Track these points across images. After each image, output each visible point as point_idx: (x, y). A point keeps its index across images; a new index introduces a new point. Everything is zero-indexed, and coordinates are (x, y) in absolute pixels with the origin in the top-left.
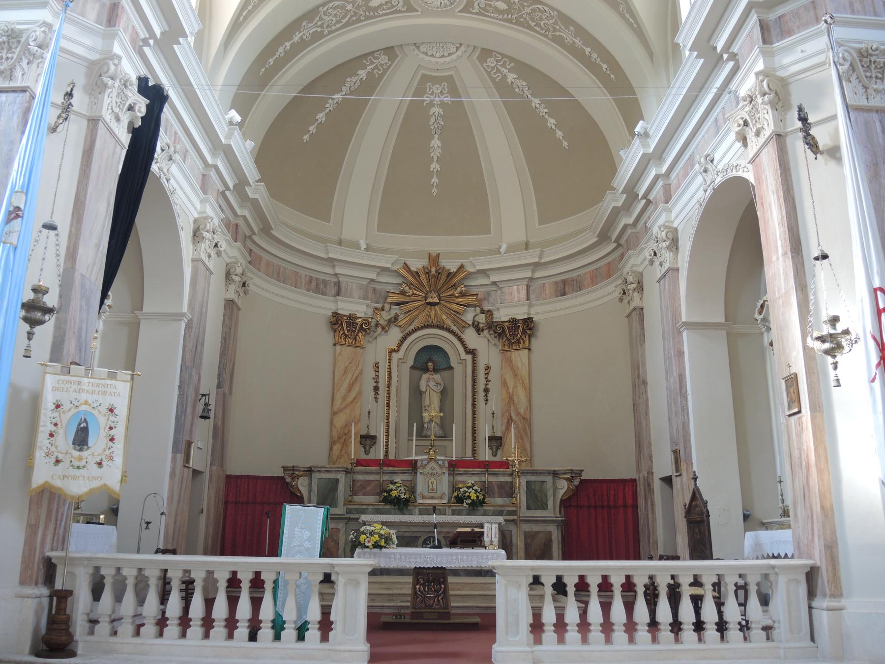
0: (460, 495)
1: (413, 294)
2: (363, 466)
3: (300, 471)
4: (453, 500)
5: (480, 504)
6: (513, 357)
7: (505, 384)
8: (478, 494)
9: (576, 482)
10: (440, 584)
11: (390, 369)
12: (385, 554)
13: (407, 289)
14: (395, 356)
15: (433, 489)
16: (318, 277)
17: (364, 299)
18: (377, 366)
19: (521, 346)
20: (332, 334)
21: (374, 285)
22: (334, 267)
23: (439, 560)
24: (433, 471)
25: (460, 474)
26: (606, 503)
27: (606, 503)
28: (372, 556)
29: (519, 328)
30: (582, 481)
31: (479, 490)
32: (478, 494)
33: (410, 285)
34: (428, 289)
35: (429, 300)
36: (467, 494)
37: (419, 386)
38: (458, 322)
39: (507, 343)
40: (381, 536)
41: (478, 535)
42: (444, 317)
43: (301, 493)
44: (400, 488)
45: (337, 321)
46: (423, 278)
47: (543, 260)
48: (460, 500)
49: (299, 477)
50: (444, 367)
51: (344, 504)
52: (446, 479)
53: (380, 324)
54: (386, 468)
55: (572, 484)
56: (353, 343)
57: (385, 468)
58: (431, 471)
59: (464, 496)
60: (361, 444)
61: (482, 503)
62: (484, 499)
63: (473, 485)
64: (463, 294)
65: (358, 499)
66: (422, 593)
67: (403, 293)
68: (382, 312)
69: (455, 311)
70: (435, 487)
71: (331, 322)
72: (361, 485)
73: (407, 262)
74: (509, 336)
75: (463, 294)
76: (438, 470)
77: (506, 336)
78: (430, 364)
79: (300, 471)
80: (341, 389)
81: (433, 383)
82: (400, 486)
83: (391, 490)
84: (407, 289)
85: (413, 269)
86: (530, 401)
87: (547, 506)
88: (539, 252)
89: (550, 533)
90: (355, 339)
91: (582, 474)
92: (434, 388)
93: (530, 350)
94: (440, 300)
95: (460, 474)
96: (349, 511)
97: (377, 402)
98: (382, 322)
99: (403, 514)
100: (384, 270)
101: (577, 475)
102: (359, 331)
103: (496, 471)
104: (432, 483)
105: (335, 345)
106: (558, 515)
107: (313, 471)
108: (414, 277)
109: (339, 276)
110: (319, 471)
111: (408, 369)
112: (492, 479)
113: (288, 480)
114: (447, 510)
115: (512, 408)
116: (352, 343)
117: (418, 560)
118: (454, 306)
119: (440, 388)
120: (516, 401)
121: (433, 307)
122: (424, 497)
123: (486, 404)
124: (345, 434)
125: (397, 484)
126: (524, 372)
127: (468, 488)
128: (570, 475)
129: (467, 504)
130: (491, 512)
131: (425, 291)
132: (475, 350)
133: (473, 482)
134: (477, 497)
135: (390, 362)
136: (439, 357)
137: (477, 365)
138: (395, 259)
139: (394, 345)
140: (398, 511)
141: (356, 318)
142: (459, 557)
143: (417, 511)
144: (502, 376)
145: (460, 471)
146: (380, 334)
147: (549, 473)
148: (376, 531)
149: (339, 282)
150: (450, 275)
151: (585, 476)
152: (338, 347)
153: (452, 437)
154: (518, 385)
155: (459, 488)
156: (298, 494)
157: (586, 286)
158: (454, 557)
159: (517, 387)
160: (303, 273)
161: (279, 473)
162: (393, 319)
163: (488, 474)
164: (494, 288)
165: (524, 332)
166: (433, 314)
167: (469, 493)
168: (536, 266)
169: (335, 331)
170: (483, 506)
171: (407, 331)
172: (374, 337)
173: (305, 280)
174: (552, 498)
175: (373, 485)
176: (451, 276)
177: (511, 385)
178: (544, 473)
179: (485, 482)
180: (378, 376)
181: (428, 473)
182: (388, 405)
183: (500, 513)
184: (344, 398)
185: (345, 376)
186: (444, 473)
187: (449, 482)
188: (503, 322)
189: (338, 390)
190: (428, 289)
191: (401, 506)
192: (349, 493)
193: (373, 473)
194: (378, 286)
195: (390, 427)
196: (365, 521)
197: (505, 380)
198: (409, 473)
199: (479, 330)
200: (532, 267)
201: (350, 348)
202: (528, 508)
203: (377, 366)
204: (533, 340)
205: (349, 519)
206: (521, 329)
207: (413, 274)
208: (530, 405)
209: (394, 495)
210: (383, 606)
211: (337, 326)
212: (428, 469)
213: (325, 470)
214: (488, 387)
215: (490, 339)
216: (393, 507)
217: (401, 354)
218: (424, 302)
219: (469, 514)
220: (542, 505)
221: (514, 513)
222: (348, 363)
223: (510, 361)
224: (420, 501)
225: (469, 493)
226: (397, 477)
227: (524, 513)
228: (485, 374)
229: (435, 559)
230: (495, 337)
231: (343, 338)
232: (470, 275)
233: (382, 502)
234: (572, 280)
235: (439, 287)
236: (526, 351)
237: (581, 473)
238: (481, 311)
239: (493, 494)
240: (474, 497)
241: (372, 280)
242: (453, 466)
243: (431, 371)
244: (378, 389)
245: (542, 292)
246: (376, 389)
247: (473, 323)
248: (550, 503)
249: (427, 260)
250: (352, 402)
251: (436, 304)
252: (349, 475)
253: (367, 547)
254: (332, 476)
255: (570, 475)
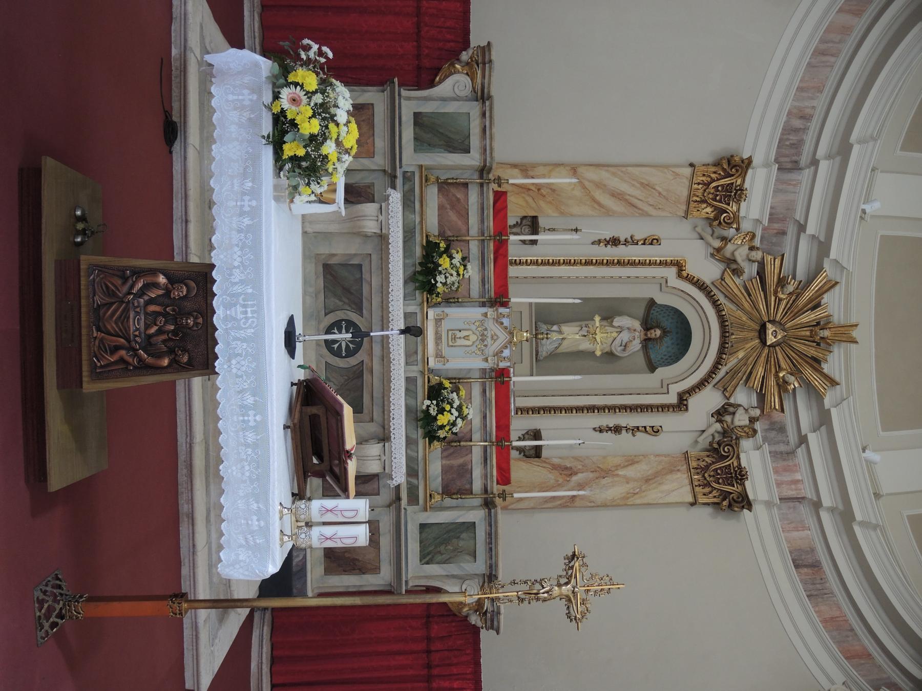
0: (445, 392)
1: (780, 300)
2: (495, 203)
3: (483, 77)
4: (435, 380)
5: (430, 432)
6: (679, 475)
7: (631, 461)
8: (447, 428)
9: (474, 619)
10: (171, 351)
11: (650, 264)
12: (255, 159)
13: (790, 288)
14: (670, 273)
15: (454, 338)
16: (810, 132)
17: (771, 214)
18: (653, 241)
19: (697, 489)
20: (710, 160)
21: (791, 230)
22: (829, 157)
23: (241, 347)
24: (489, 340)
25: (484, 391)
26: (435, 672)
27: (435, 672)
28: (246, 114)
29: (729, 485)
30: (476, 631)
31: (454, 430)
32: (447, 428)
33: (797, 294)
34: (789, 325)
35: (770, 328)
36: (448, 407)
37: (620, 314)
38: (732, 378)
39: (703, 464)
40: (315, 141)
41: (337, 470)
42: (741, 354)
43: (440, 82)
44: (455, 274)
45: (735, 166)
46: (809, 317)
47: (857, 529)
48: (435, 392)
49: (472, 76)
50: (652, 356)
51: (421, 167)
52: (476, 363)
53: (726, 244)
54: (492, 248)
55: (471, 612)
56: (695, 198)
57: (492, 245)
58: (489, 335)
59: (443, 401)
60: (524, 218)
61: (431, 436)
62: (439, 439)
63: (464, 418)
64: (782, 386)
65: (433, 196)
66: (142, 293)
67: (782, 282)
68: (747, 247)
69: (751, 373)
70: (460, 342)
71: (732, 156)
72: (458, 200)
73: (837, 288)
74: (713, 467)
75: (782, 386)
76: (493, 347)
77: (713, 463)
78: (658, 332)
79: (483, 77)
80: (616, 179)
81: (626, 339)
82: (458, 275)
83: (451, 257)
84: (790, 288)
85: (826, 298)
86: (604, 506)
87: (427, 563)
88: (874, 522)
89: (376, 570)
90: (703, 201)
91: (491, 631)
92: (617, 342)
93: (692, 504)
94: (769, 346)
95: (484, 391)
96: (408, 178)
97: (593, 243)
98: (730, 247)
99: (406, 282)
100: (823, 248)
101: (489, 623)
102: (716, 208)
103: (491, 461)
104: (466, 338)
105: (692, 165)
106: (411, 584)
107: (484, 102)
108: (810, 300)
109: (813, 168)
110: (484, 115)
111: (648, 295)
112: (477, 454)
113: (465, 56)
114: (414, 368)
115: (591, 475)
116: (695, 195)
117: (237, 276)
118: (760, 371)
119: (617, 350)
120: (604, 481)
121: (757, 334)
122: (438, 321)
123: (594, 429)
124: (539, 190)
125: (462, 268)
126: (653, 495)
127: (459, 409)
128: (490, 609)
129: (428, 406)
130: (414, 454)
131: (785, 320)
132: (687, 410)
133: (470, 417)
134: (442, 427)
135: (661, 263)
136: (668, 347)
137: (661, 414)
138: (845, 265)
139: (691, 269)
140: (410, 271)
141: (738, 202)
142: (251, 418)
143: (412, 308)
144: (645, 456)
145: (491, 392)
146: (708, 244)
147: (491, 567)
148: (332, 126)
149: (800, 169)
150: (815, 363)
151: (484, 634)
152: (688, 171)
153: (538, 375)
154: (630, 486)
155: (457, 390)
156: (438, 78)
157: (817, 609)
158: (250, 400)
159: (628, 483)
160: (820, 103)
161: (476, 39)
162: (734, 266)
163: (485, 447)
164: (792, 437)
165: (725, 495)
166: (745, 334)
167: (450, 411)
168: (846, 516)
169: (717, 164)
170: (424, 438)
171: (715, 291)
172: (703, 234)
173: (807, 107)
174: (445, 573)
175: (460, 223)
176: (815, 365)
177: (630, 472)
178: (491, 558)
179: (471, 441)
180: (637, 244)
181: (486, 329)
182: (588, 263)
183: (412, 472)
184: (600, 185)
185: (638, 185)
186: (486, 360)
187: (470, 370)
188: (738, 458)
189: (614, 174)
190: (789, 325)
191: (420, 278)
192: (443, 178)
193: (482, 221)
194: (789, 239)
195: (552, 268)
196: (388, 199)
197: (638, 462)
198: (482, 294)
199: (720, 414)
200: (841, 507)
201: (685, 193)
202: (423, 527)
203: (653, 241)
204: (709, 510)
205: (394, 177)
206: (728, 488)
207: (817, 298)
208: (598, 506)
209: (441, 261)
210: (187, 221)
211: (725, 166)
212: (494, 328)
213: (485, 126)
214: (624, 431)
215: (705, 435)
216: (418, 261)
217: (674, 282)
218: (766, 320)
219: (409, 410)
220: (428, 554)
221: (413, 499)
222: (660, 190)
223: (671, 470)
224: (432, 313)
225: (450, 411)
226: (476, 269)
227: (414, 517)
228: (645, 427)
229: (241, 334)
230: (711, 444)
231: (704, 178)
232: (816, 395)
233: (428, 242)
234: (823, 580)
235: (792, 343)
236: (691, 499)
237: (492, 628)
238: (754, 418)
239: (447, 457)
240: (443, 419)
241: (802, 228)
242: (500, 377)
243: (646, 335)
244: (616, 245)
245: (793, 525)
246: (615, 242)
247: (731, 405)
248: (434, 569)
249: (842, 322)
250: (594, 200)
251: (763, 341)
252: (476, 176)
253: (276, 97)
254: (475, 141)
255: (490, 609)
